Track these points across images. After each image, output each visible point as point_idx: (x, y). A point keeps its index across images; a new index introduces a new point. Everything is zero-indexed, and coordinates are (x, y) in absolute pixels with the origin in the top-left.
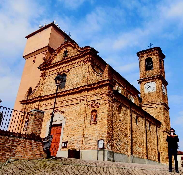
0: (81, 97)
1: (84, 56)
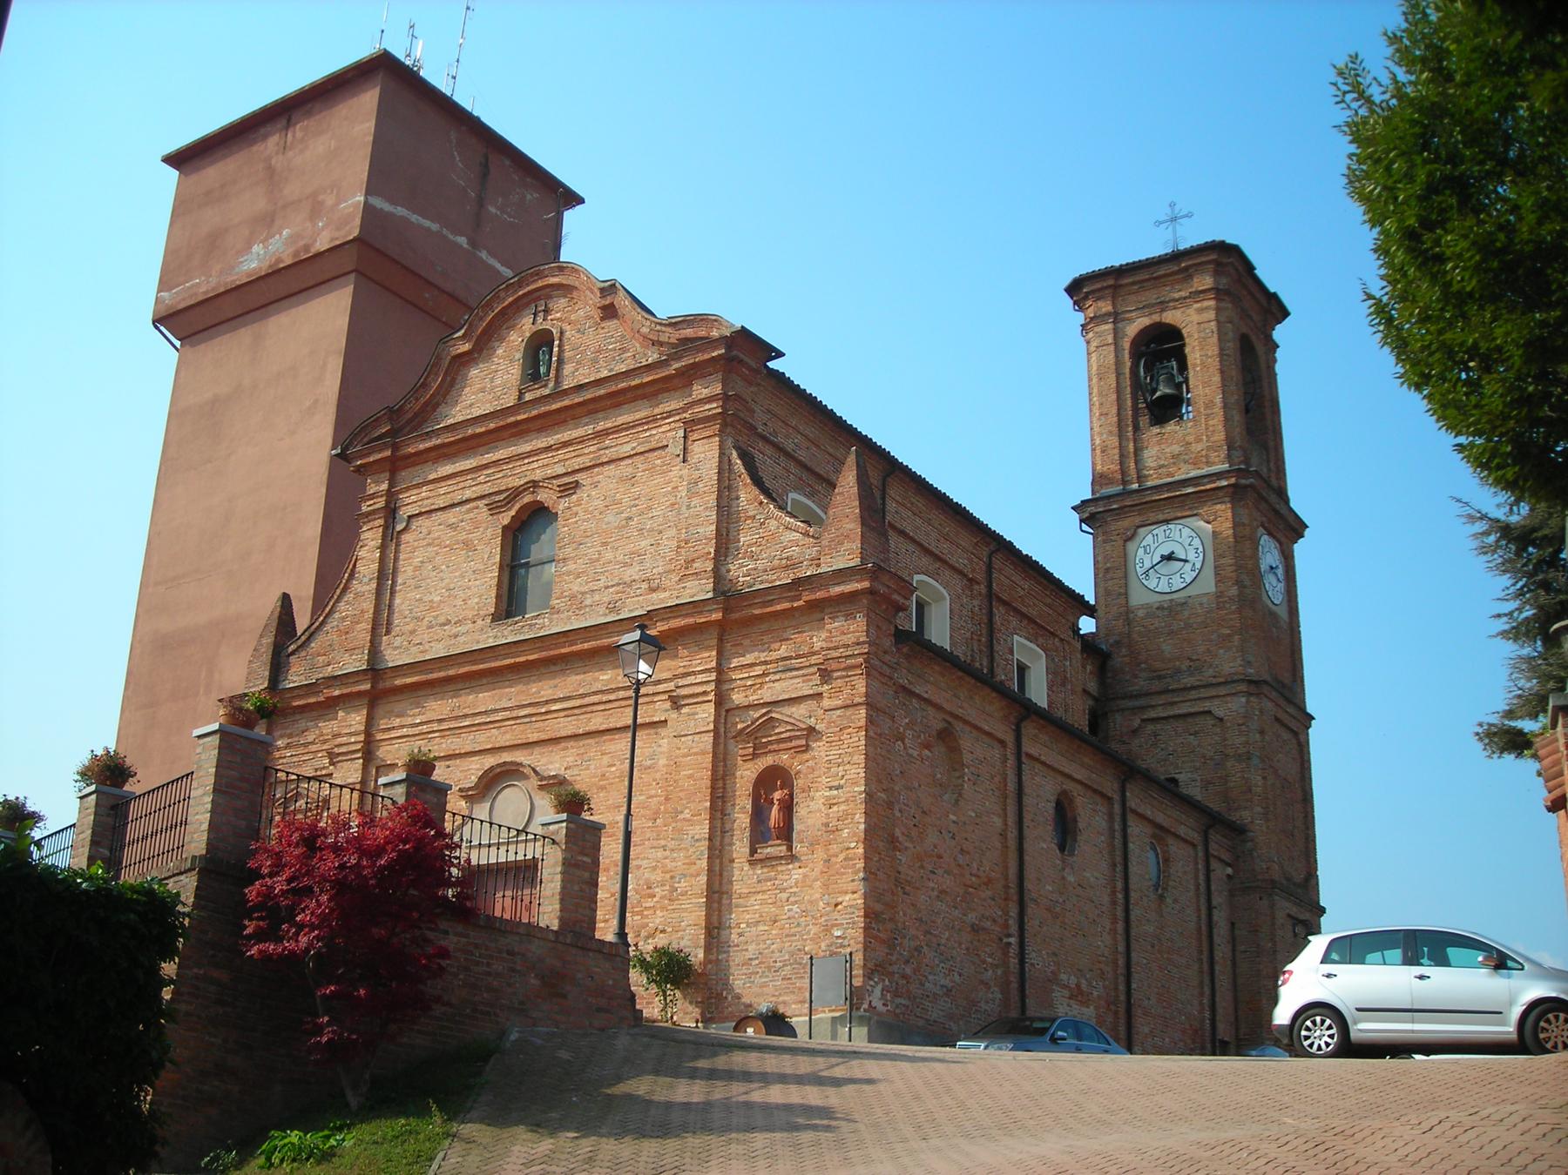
0: (676, 677)
1: (687, 377)
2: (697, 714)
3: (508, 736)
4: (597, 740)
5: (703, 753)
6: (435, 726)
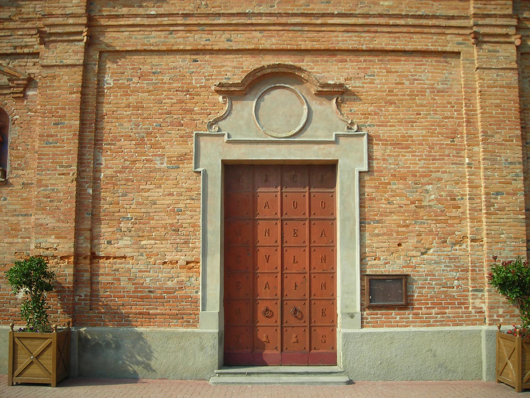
2: (498, 52)
3: (274, 40)
4: (380, 58)
5: (509, 87)
6: (180, 20)
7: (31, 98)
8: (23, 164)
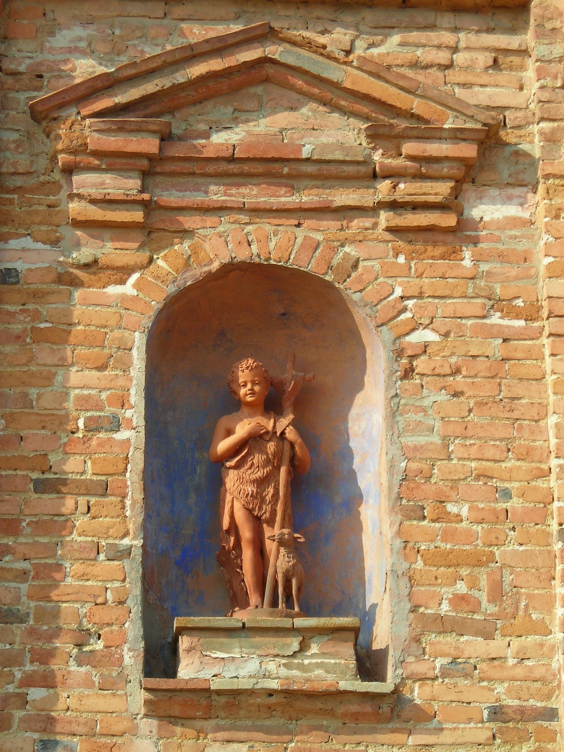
7: (499, 240)
8: (484, 597)
